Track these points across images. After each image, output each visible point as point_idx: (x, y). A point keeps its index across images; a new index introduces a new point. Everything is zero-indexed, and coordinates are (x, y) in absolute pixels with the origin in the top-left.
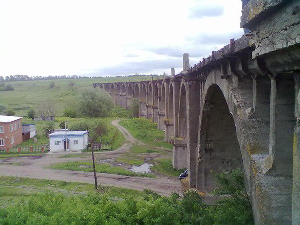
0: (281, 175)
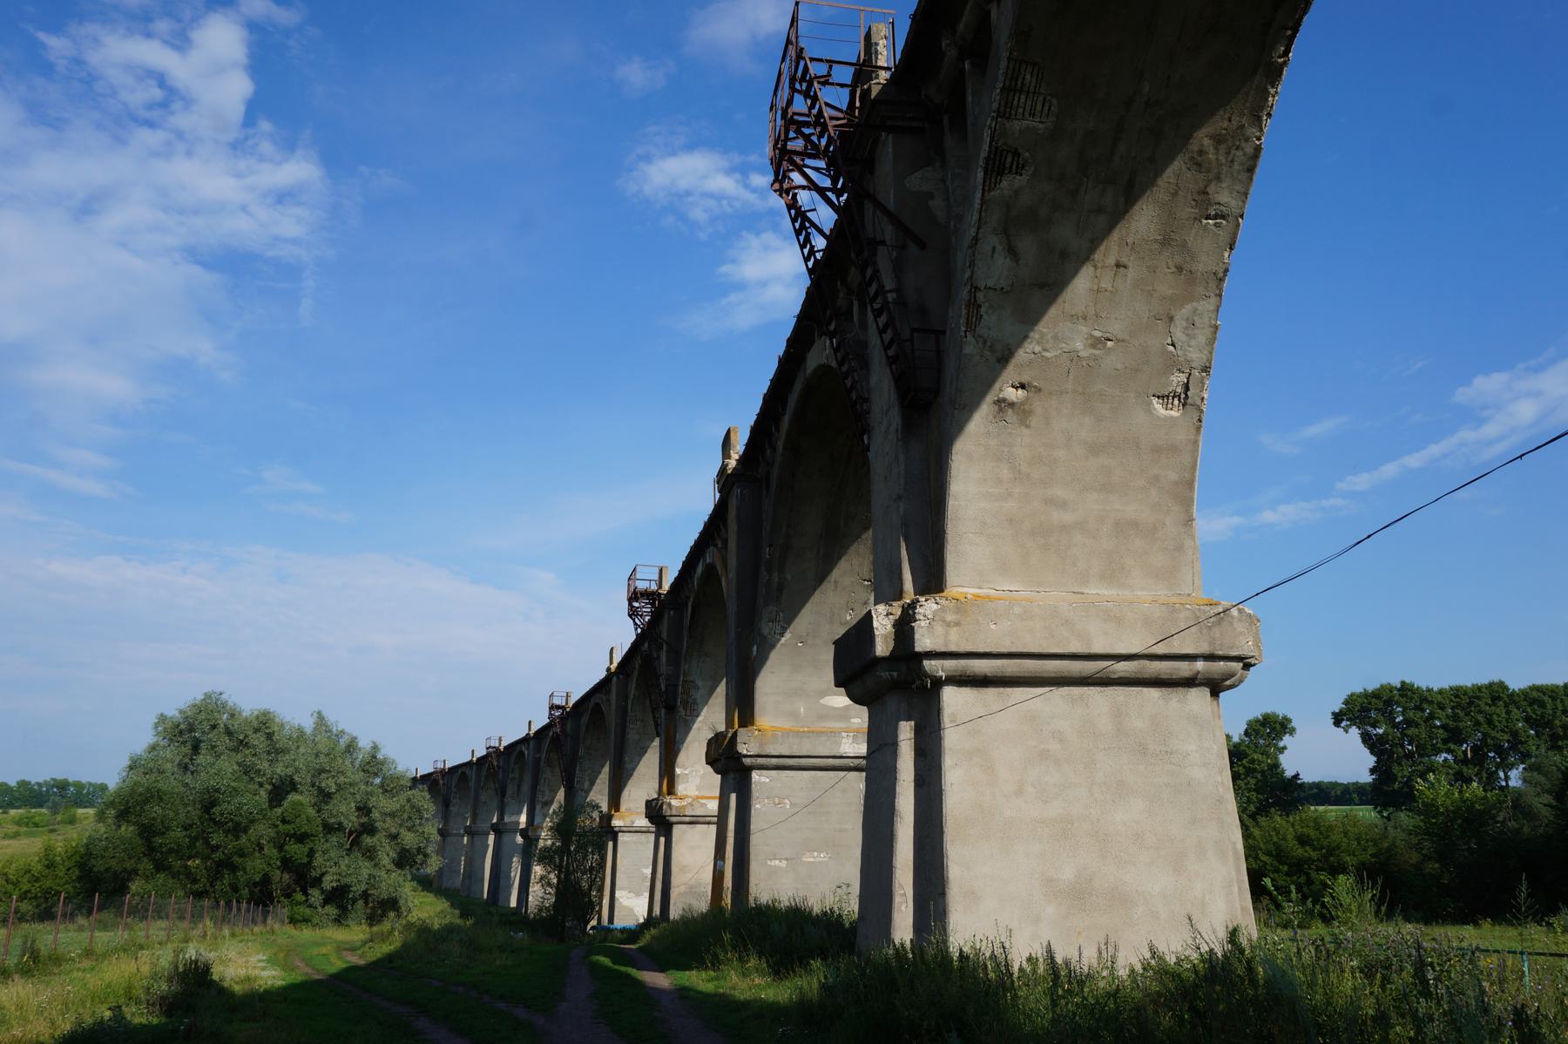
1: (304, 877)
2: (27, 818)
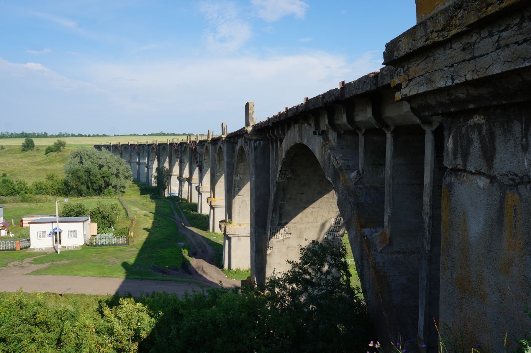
0: (399, 252)
1: (108, 184)
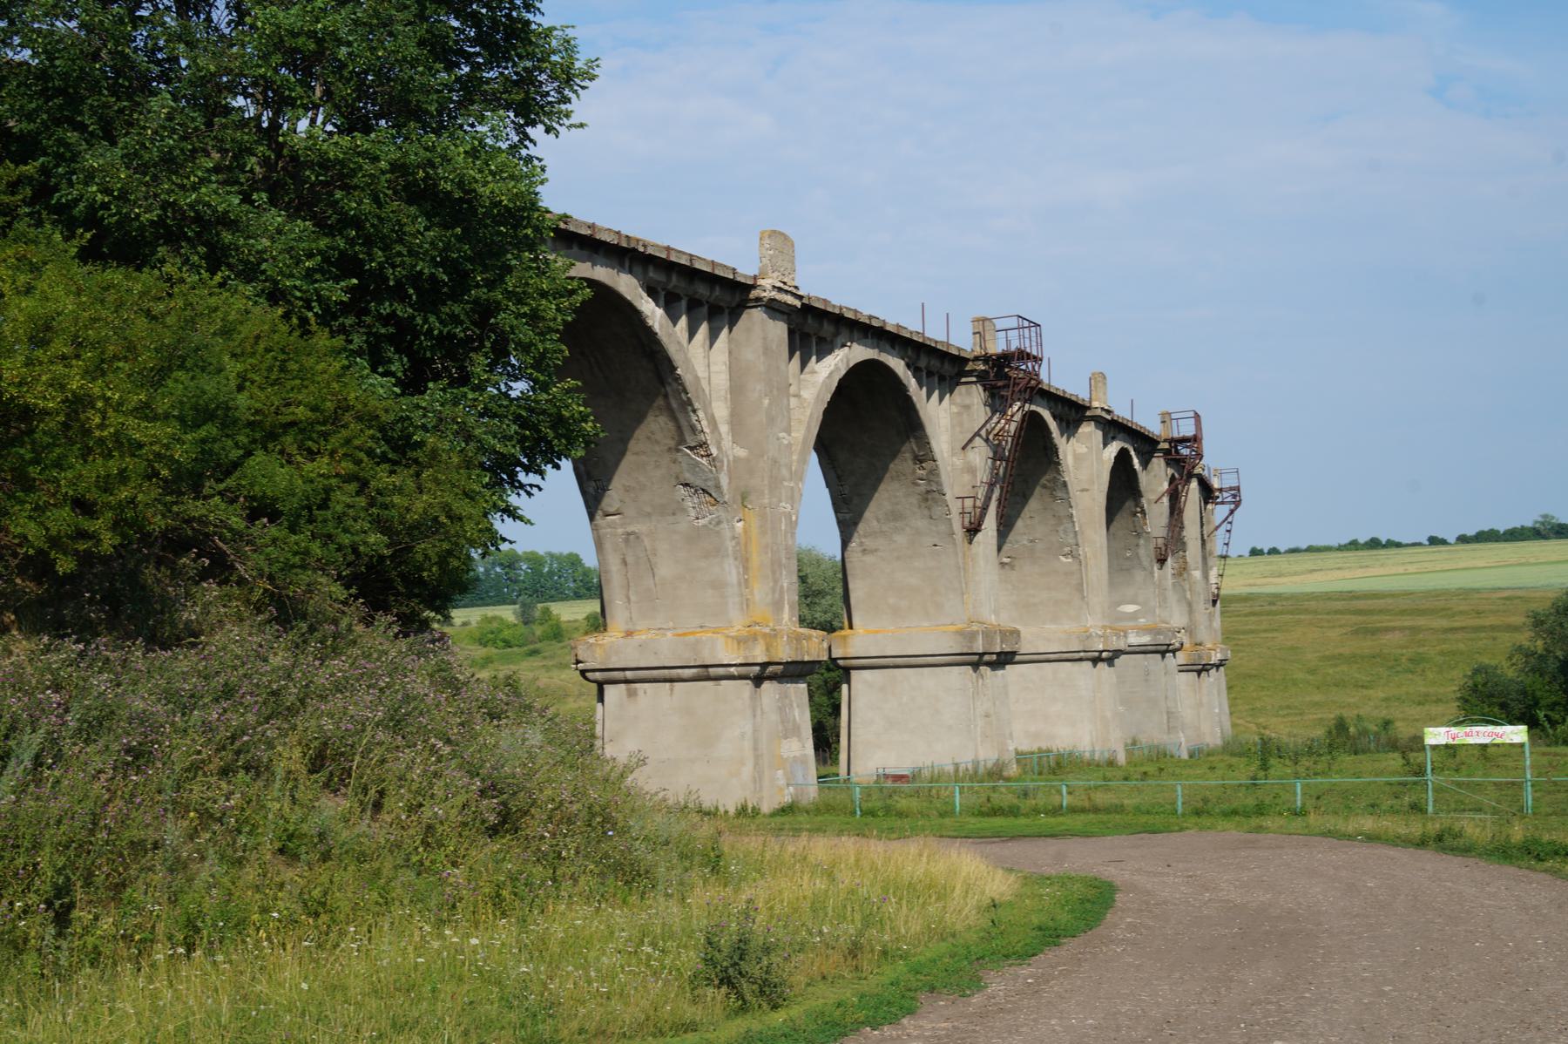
2: (492, 633)
